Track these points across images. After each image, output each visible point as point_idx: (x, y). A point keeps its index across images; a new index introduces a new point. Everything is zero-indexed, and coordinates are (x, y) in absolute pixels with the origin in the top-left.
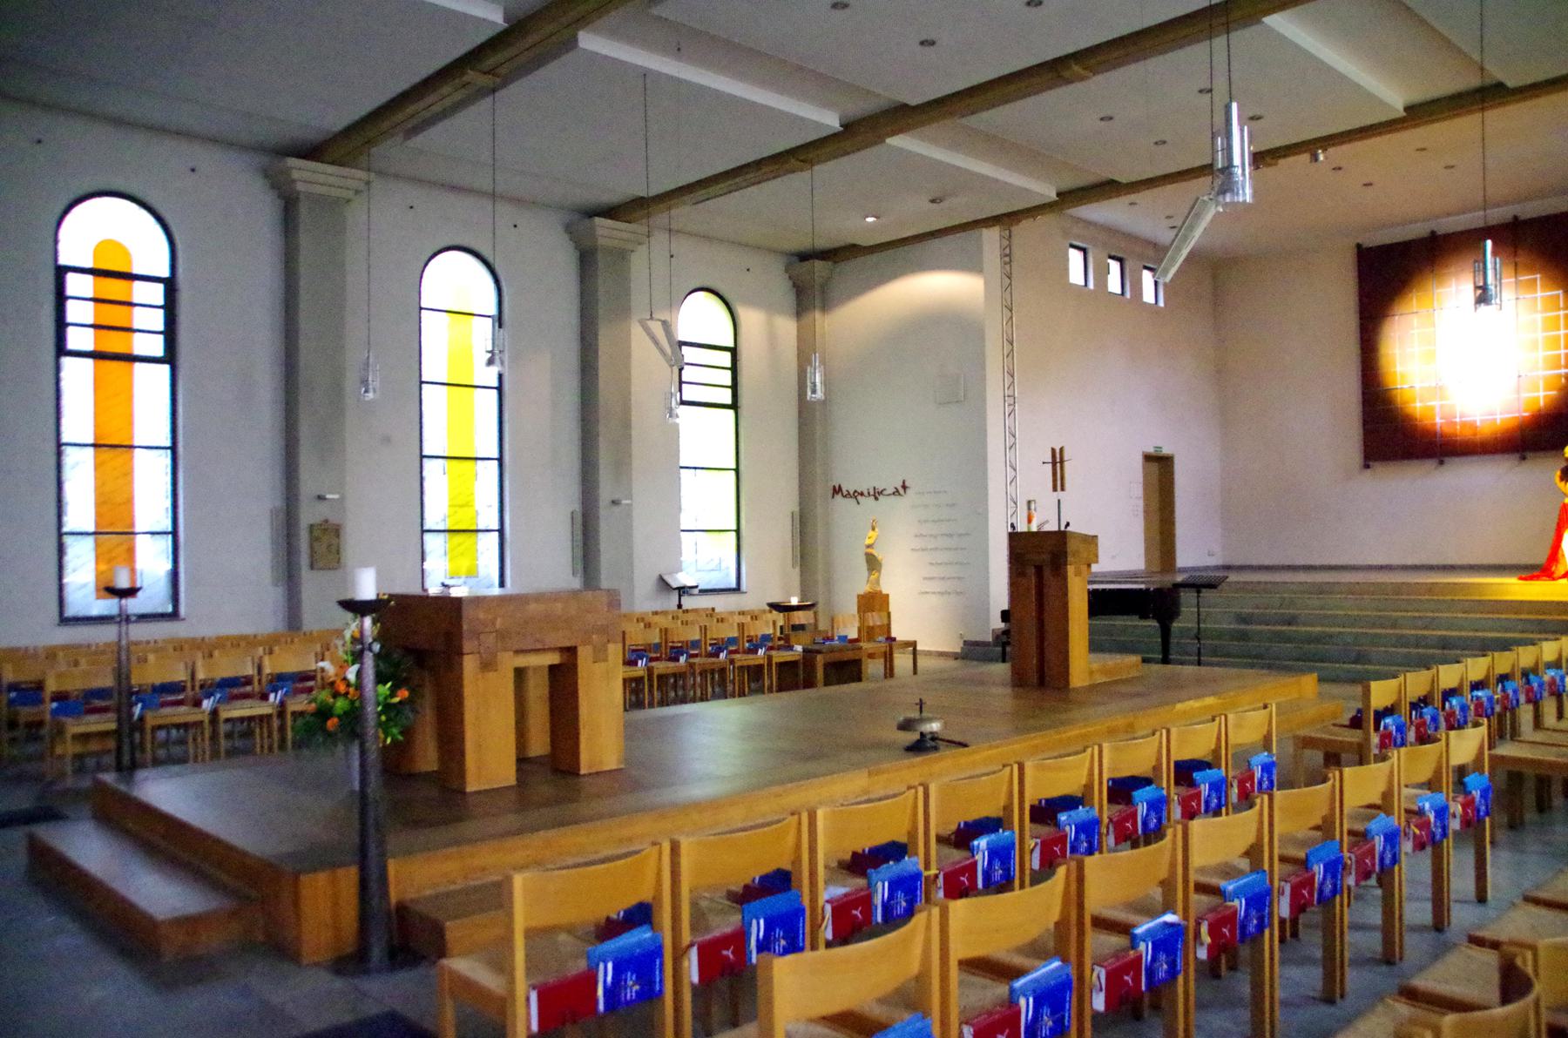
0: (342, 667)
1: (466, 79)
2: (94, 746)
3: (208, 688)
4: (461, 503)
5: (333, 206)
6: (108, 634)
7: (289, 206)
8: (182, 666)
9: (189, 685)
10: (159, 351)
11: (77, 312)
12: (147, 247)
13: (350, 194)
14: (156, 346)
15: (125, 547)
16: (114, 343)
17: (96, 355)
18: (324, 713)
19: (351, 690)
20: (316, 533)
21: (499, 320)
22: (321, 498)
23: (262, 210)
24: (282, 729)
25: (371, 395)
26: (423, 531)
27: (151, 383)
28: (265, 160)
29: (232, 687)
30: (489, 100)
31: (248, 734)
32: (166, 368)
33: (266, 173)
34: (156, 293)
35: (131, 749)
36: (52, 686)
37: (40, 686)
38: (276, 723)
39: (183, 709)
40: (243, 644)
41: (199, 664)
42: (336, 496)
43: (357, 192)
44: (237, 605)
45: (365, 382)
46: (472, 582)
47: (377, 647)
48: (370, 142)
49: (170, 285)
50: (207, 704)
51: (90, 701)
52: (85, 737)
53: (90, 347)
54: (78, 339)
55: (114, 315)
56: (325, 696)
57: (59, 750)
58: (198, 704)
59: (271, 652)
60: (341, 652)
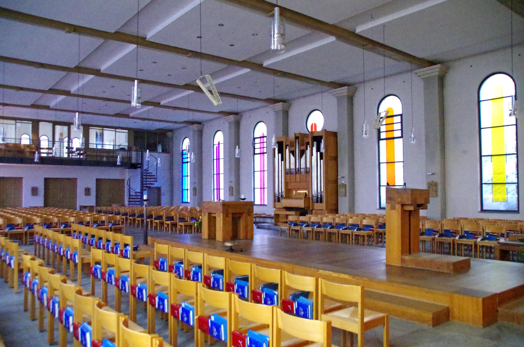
16: (390, 135)
17: (387, 139)
53: (385, 137)
54: (257, 151)
55: (390, 128)
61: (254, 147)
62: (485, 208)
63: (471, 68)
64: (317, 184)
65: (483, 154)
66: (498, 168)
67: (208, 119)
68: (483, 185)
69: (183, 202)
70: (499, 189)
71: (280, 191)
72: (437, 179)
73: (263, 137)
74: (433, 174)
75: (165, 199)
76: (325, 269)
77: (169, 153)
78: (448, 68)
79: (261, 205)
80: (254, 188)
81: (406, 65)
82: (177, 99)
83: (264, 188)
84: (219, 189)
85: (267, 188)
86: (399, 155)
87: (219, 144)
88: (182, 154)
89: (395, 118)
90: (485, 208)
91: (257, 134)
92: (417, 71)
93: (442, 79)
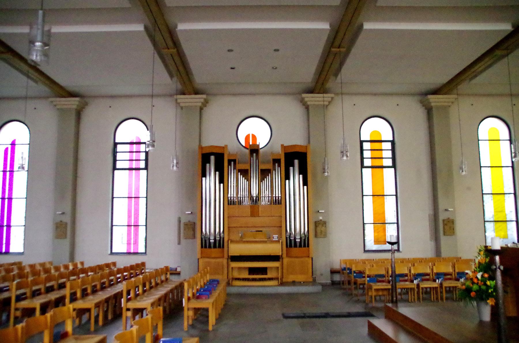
0: (475, 272)
1: (495, 54)
2: (380, 293)
3: (417, 276)
4: (500, 210)
5: (445, 109)
6: (388, 256)
7: (429, 111)
8: (406, 268)
9: (387, 275)
10: (390, 164)
11: (367, 154)
12: (385, 131)
13: (450, 104)
14: (389, 162)
15: (382, 228)
16: (377, 163)
17: (372, 167)
18: (468, 290)
19: (479, 282)
20: (445, 222)
21: (510, 140)
22: (446, 210)
23: (420, 114)
24: (441, 292)
25: (464, 173)
26: (485, 221)
27: (389, 174)
28: (419, 98)
29: (422, 276)
30: (506, 58)
31: (407, 293)
32: (393, 169)
33: (421, 102)
34: (389, 146)
35: (394, 296)
36: (367, 273)
37: (364, 273)
38: (416, 290)
39: (407, 283)
40: (404, 262)
41: (412, 268)
42: (452, 209)
43: (452, 103)
44: (417, 247)
45: (461, 168)
46: (505, 240)
47: (502, 268)
48: (457, 85)
49: (393, 142)
50: (415, 282)
51: (377, 278)
52: (377, 290)
53: (370, 165)
54: (367, 162)
55: (377, 154)
56: (468, 283)
57: (370, 294)
58: (412, 281)
59: (414, 265)
60: (473, 267)
62: (114, 251)
63: (355, 106)
66: (497, 207)
69: (146, 253)
70: (500, 226)
72: (67, 219)
73: (139, 143)
74: (63, 213)
78: (86, 104)
79: (129, 253)
80: (112, 226)
85: (3, 226)
86: (389, 187)
89: (383, 143)
90: (114, 251)
91: (366, 133)
93: (79, 114)
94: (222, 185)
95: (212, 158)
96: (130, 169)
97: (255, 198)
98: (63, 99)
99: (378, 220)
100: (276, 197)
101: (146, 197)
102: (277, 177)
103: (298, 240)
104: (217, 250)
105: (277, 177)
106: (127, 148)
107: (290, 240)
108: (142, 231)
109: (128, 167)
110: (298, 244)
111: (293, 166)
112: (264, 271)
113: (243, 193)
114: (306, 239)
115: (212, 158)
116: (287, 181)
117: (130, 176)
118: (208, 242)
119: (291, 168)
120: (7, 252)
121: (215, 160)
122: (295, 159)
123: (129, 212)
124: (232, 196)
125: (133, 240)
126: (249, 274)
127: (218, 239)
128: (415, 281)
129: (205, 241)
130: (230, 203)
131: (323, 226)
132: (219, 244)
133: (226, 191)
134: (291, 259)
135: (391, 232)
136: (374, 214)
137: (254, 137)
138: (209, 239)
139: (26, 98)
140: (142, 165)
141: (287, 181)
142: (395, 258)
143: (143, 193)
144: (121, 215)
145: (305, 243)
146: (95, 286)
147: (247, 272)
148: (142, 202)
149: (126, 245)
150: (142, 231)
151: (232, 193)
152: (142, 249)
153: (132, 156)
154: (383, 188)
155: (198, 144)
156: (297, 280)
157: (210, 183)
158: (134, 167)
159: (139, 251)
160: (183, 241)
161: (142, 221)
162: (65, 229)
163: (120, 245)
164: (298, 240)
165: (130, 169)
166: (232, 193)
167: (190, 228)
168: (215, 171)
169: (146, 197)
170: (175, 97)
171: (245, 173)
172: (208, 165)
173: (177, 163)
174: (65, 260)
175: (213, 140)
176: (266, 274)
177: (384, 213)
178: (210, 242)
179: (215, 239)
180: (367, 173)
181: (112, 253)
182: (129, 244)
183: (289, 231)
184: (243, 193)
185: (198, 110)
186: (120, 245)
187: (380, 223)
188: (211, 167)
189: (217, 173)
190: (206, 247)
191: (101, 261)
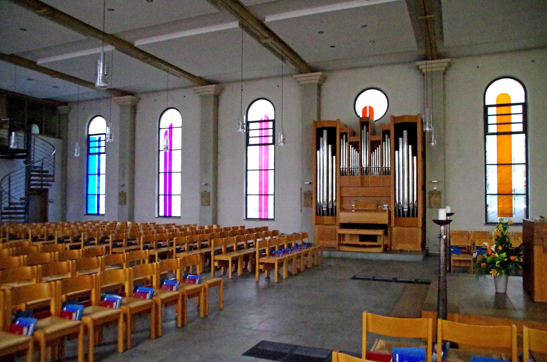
11: (492, 120)
14: (520, 128)
16: (504, 129)
17: (498, 134)
34: (520, 109)
53: (495, 131)
54: (492, 129)
61: (88, 145)
62: (248, 217)
63: (479, 69)
64: (406, 191)
65: (487, 163)
67: (86, 97)
68: (488, 196)
71: (330, 199)
72: (126, 189)
73: (267, 121)
74: (206, 184)
75: (53, 210)
76: (157, 278)
77: (59, 137)
78: (223, 89)
79: (260, 219)
81: (187, 81)
82: (61, 62)
83: (267, 195)
84: (170, 195)
87: (171, 128)
88: (88, 141)
90: (248, 217)
92: (195, 88)
93: (217, 98)
94: (334, 157)
95: (325, 132)
96: (261, 145)
97: (365, 169)
98: (203, 87)
99: (82, 192)
100: (385, 168)
101: (274, 170)
102: (387, 147)
103: (406, 210)
104: (330, 218)
105: (387, 147)
106: (257, 126)
107: (399, 210)
108: (271, 199)
109: (258, 143)
110: (406, 214)
111: (402, 136)
112: (374, 238)
113: (355, 164)
114: (415, 209)
115: (325, 132)
116: (397, 152)
117: (261, 150)
118: (401, 211)
119: (400, 139)
120: (170, 216)
121: (329, 134)
122: (404, 129)
123: (260, 183)
124: (387, 166)
125: (263, 207)
126: (361, 240)
127: (411, 208)
128: (474, 254)
129: (399, 210)
130: (342, 173)
131: (436, 196)
132: (332, 212)
133: (338, 162)
134: (400, 228)
135: (519, 205)
136: (498, 184)
137: (371, 109)
138: (403, 208)
139: (167, 90)
140: (270, 140)
141: (397, 152)
142: (451, 229)
143: (271, 166)
144: (253, 187)
145: (412, 213)
146: (274, 249)
147: (358, 238)
148: (271, 174)
149: (258, 212)
150: (271, 199)
151: (344, 164)
152: (271, 216)
153: (262, 132)
154: (511, 156)
155: (483, 104)
156: (406, 249)
157: (323, 154)
158: (263, 143)
159: (269, 218)
160: (303, 208)
161: (271, 191)
162: (210, 198)
163: (253, 212)
164: (406, 210)
165: (261, 145)
166: (344, 164)
167: (309, 196)
168: (328, 145)
169: (274, 170)
170: (295, 76)
171: (357, 146)
172: (321, 139)
173: (284, 139)
174: (210, 221)
175: (330, 115)
176: (376, 242)
177: (510, 183)
178: (403, 212)
179: (409, 208)
180: (492, 141)
181: (247, 219)
182: (260, 211)
183: (397, 201)
184: (355, 164)
185: (316, 87)
186: (253, 212)
187: (505, 194)
188: (324, 141)
189: (330, 146)
190: (320, 215)
191: (238, 224)
